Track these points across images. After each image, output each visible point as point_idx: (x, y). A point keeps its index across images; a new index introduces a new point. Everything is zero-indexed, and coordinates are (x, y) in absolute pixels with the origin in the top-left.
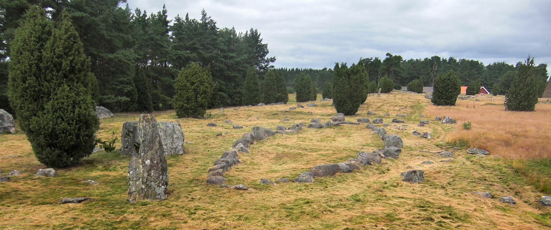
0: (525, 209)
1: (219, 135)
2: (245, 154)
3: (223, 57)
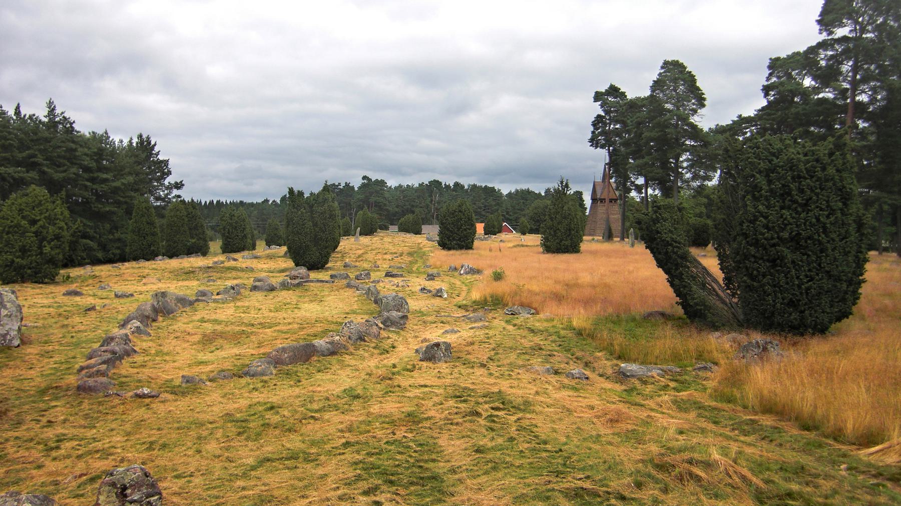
0: (603, 385)
1: (89, 310)
2: (145, 338)
3: (87, 180)
